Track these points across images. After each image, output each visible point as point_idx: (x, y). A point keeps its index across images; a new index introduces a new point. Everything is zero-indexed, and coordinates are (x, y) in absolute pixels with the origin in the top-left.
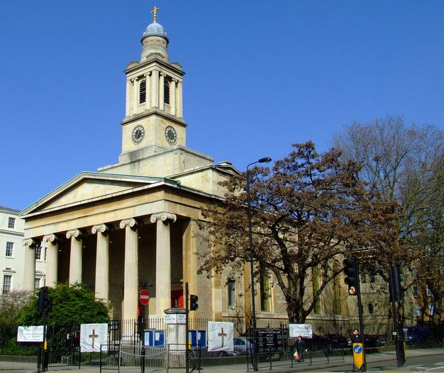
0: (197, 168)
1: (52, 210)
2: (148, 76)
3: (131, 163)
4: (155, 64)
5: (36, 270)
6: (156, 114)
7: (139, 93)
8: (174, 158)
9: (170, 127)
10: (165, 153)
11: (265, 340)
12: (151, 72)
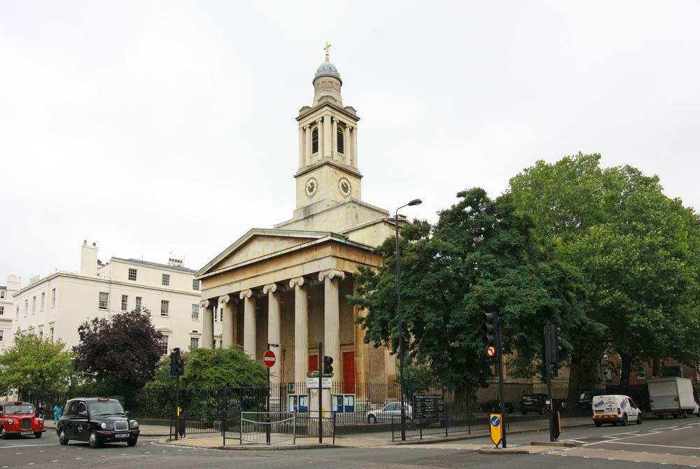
0: (370, 221)
1: (225, 270)
2: (320, 123)
3: (305, 218)
4: (327, 108)
6: (328, 164)
9: (344, 178)
10: (337, 207)
11: (423, 406)
12: (323, 118)
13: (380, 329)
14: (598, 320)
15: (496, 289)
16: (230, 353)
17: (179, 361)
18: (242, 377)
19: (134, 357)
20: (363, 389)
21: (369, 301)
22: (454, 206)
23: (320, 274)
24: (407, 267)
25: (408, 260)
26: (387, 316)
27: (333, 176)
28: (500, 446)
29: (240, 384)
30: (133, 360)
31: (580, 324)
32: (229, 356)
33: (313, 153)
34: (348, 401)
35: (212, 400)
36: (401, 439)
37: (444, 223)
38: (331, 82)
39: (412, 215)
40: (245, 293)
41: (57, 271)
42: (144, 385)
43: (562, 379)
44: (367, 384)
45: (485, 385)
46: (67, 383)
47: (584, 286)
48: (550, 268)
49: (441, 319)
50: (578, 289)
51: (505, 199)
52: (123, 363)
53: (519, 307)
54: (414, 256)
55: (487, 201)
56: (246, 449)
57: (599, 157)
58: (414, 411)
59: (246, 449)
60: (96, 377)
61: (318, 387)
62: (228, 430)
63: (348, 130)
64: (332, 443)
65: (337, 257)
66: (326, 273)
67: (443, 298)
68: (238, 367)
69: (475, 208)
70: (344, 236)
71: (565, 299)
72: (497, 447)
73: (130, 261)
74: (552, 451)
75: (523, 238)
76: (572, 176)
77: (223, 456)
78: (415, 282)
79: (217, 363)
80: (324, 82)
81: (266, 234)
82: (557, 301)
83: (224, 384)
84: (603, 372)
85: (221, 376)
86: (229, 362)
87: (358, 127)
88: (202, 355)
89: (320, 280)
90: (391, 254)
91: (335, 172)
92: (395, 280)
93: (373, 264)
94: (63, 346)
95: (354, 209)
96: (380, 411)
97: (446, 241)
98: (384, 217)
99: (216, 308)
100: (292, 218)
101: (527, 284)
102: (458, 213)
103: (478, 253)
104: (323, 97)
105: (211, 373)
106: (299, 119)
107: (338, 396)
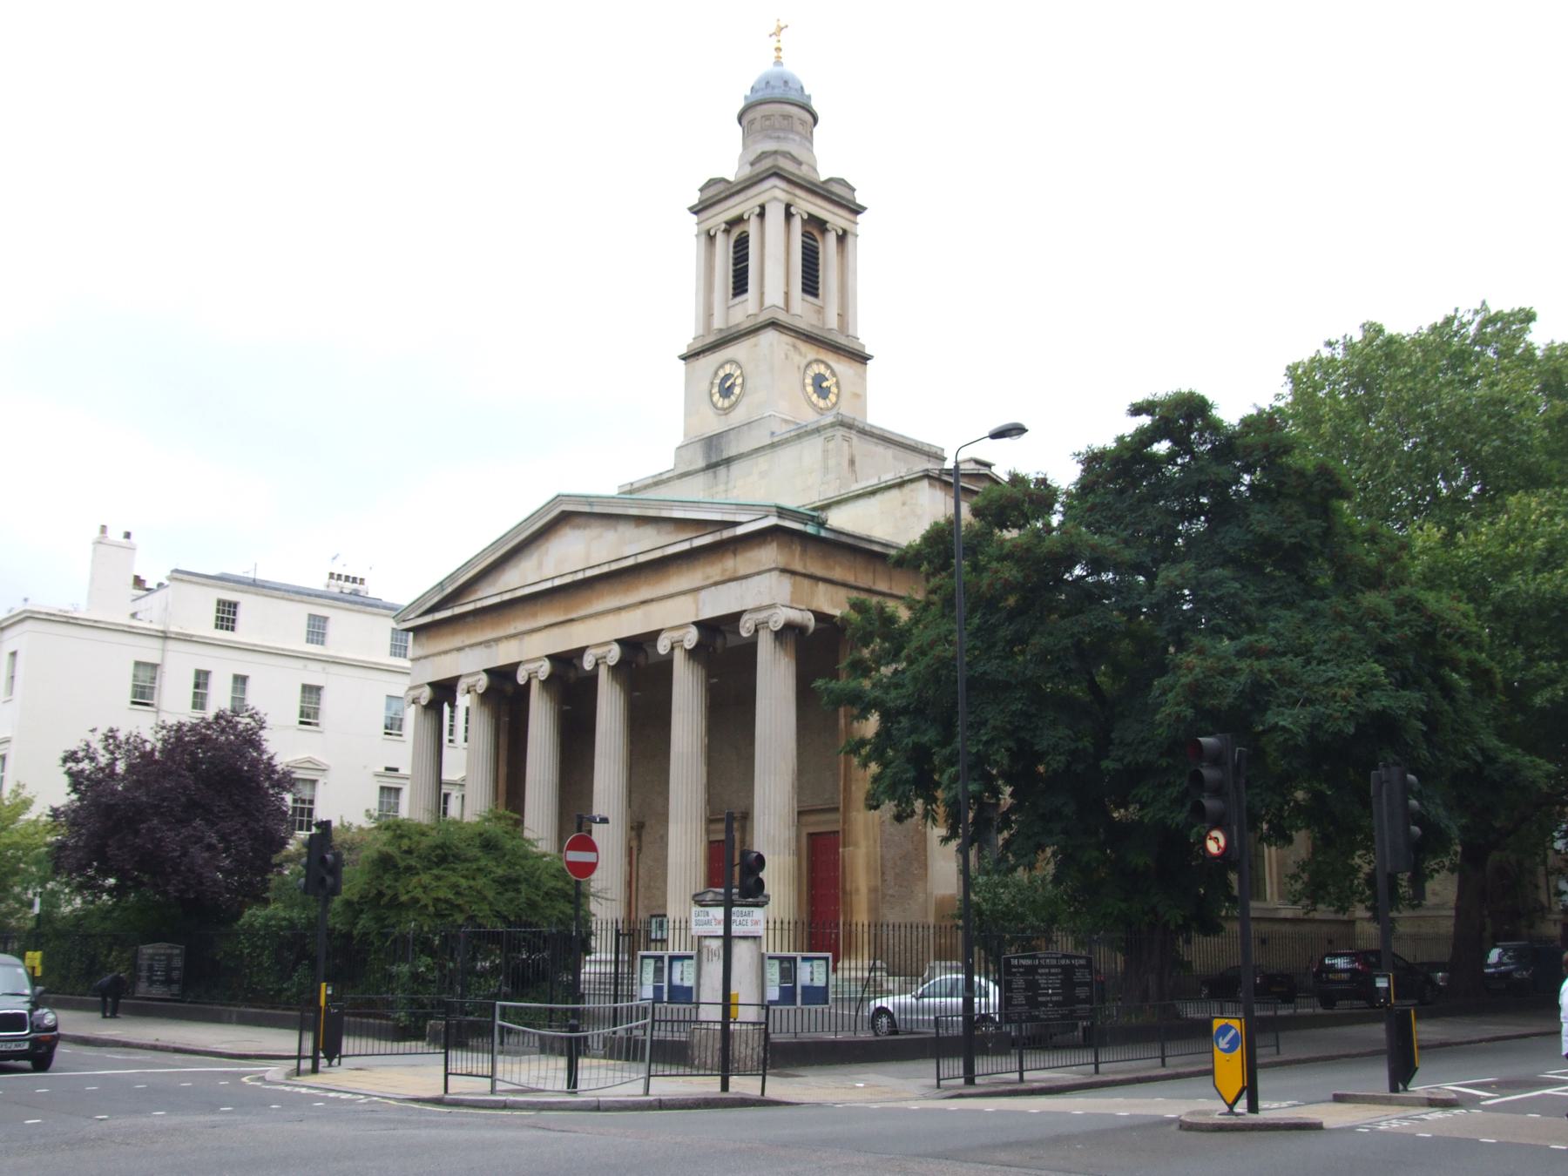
0: (889, 477)
1: (479, 605)
5: (446, 776)
6: (774, 324)
7: (731, 268)
8: (825, 451)
10: (799, 437)
11: (1032, 986)
12: (762, 207)
13: (910, 775)
14: (1530, 749)
15: (1243, 665)
16: (481, 835)
17: (329, 856)
18: (511, 901)
19: (214, 841)
20: (863, 938)
21: (877, 693)
22: (1120, 439)
23: (745, 617)
24: (986, 603)
25: (991, 585)
26: (929, 736)
27: (787, 357)
28: (1242, 1106)
29: (505, 919)
30: (210, 847)
31: (1479, 758)
32: (477, 842)
33: (735, 295)
34: (810, 973)
35: (423, 963)
36: (962, 1081)
37: (1095, 483)
38: (787, 117)
39: (1006, 460)
40: (532, 666)
41: (28, 607)
42: (239, 915)
43: (1437, 907)
44: (876, 926)
45: (1210, 927)
46: (31, 905)
47: (1491, 657)
48: (1392, 609)
49: (1086, 743)
50: (1472, 663)
51: (1261, 423)
52: (185, 854)
53: (1304, 715)
54: (1010, 572)
55: (1215, 426)
56: (505, 1106)
57: (1529, 317)
58: (1005, 1001)
59: (505, 1106)
60: (110, 891)
61: (721, 932)
62: (462, 1045)
63: (831, 239)
64: (759, 1093)
65: (793, 573)
66: (762, 616)
67: (1094, 688)
68: (500, 872)
69: (1182, 444)
70: (815, 516)
71: (1437, 694)
72: (1231, 1112)
73: (223, 579)
74: (1390, 1120)
75: (1317, 526)
76: (1461, 358)
77: (437, 1125)
78: (1011, 643)
79: (442, 860)
80: (767, 117)
81: (597, 509)
82: (1413, 698)
83: (460, 919)
84: (1552, 891)
85: (451, 896)
86: (477, 859)
87: (860, 230)
88: (401, 837)
89: (744, 634)
90: (946, 566)
91: (794, 346)
92: (956, 637)
93: (895, 592)
94: (27, 804)
95: (845, 445)
96: (907, 999)
97: (1099, 531)
98: (929, 466)
99: (453, 706)
100: (672, 467)
101: (1328, 652)
102: (1132, 457)
103: (1189, 565)
104: (763, 156)
105: (425, 888)
106: (697, 210)
107: (782, 959)
